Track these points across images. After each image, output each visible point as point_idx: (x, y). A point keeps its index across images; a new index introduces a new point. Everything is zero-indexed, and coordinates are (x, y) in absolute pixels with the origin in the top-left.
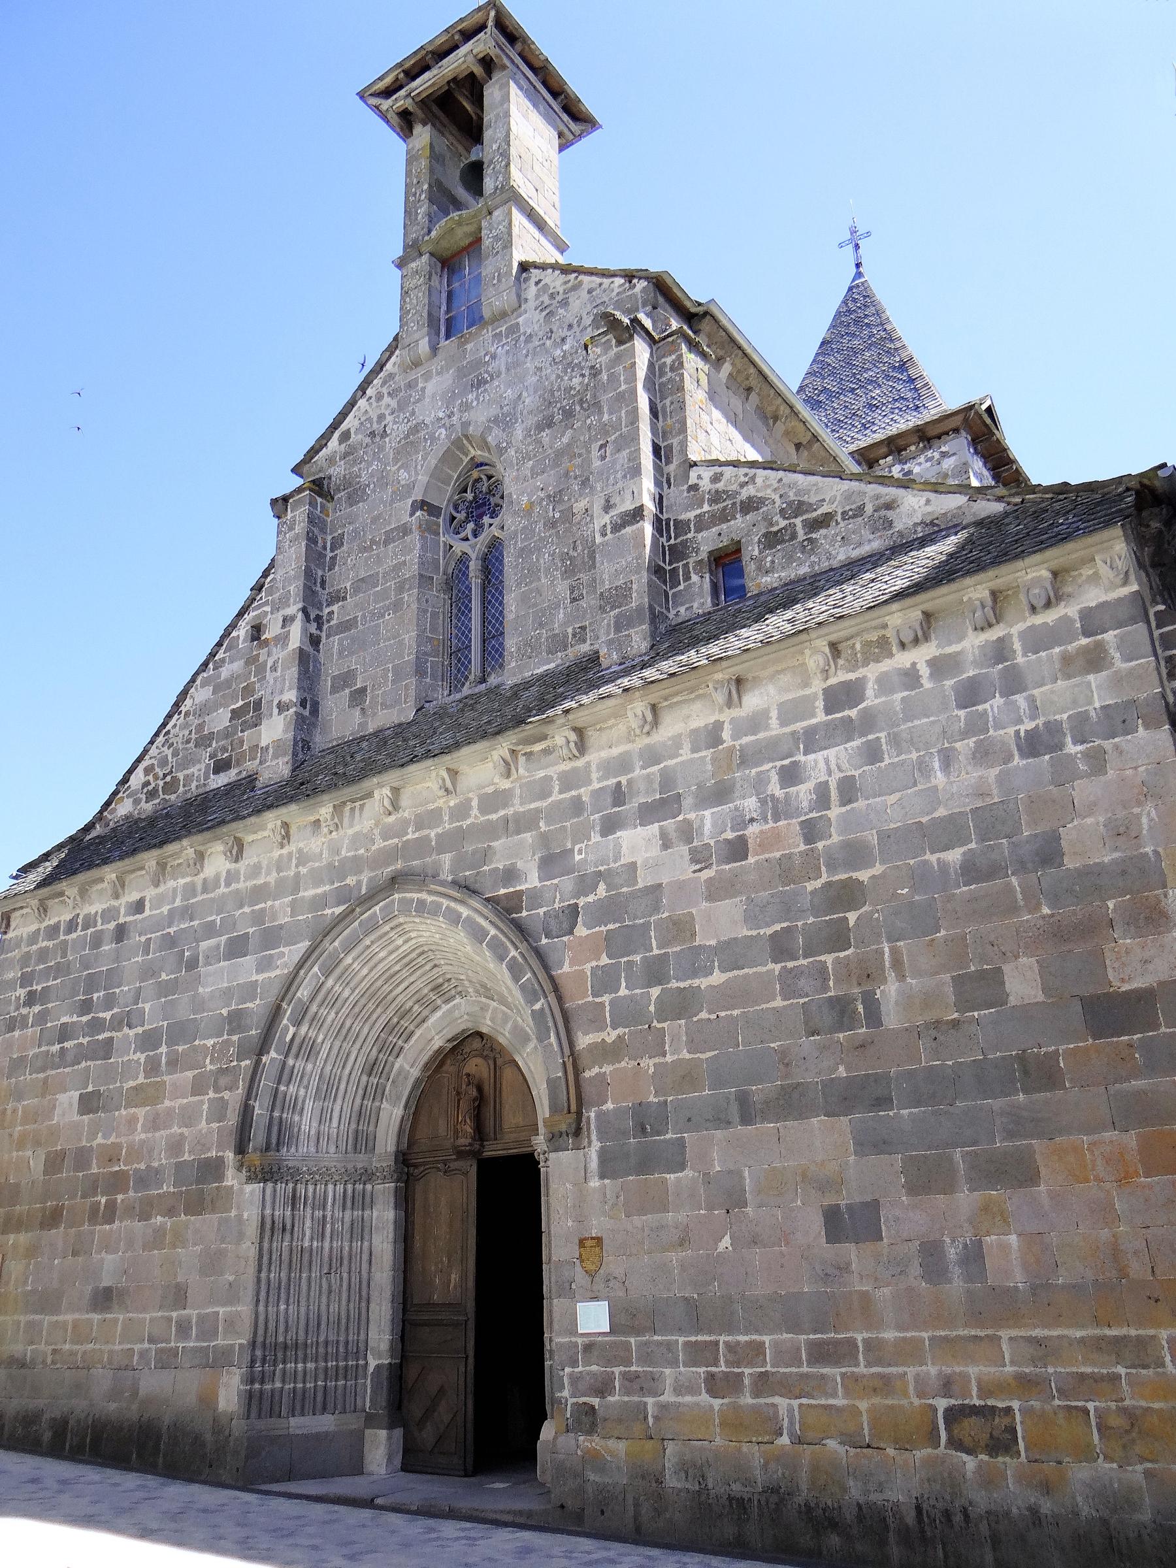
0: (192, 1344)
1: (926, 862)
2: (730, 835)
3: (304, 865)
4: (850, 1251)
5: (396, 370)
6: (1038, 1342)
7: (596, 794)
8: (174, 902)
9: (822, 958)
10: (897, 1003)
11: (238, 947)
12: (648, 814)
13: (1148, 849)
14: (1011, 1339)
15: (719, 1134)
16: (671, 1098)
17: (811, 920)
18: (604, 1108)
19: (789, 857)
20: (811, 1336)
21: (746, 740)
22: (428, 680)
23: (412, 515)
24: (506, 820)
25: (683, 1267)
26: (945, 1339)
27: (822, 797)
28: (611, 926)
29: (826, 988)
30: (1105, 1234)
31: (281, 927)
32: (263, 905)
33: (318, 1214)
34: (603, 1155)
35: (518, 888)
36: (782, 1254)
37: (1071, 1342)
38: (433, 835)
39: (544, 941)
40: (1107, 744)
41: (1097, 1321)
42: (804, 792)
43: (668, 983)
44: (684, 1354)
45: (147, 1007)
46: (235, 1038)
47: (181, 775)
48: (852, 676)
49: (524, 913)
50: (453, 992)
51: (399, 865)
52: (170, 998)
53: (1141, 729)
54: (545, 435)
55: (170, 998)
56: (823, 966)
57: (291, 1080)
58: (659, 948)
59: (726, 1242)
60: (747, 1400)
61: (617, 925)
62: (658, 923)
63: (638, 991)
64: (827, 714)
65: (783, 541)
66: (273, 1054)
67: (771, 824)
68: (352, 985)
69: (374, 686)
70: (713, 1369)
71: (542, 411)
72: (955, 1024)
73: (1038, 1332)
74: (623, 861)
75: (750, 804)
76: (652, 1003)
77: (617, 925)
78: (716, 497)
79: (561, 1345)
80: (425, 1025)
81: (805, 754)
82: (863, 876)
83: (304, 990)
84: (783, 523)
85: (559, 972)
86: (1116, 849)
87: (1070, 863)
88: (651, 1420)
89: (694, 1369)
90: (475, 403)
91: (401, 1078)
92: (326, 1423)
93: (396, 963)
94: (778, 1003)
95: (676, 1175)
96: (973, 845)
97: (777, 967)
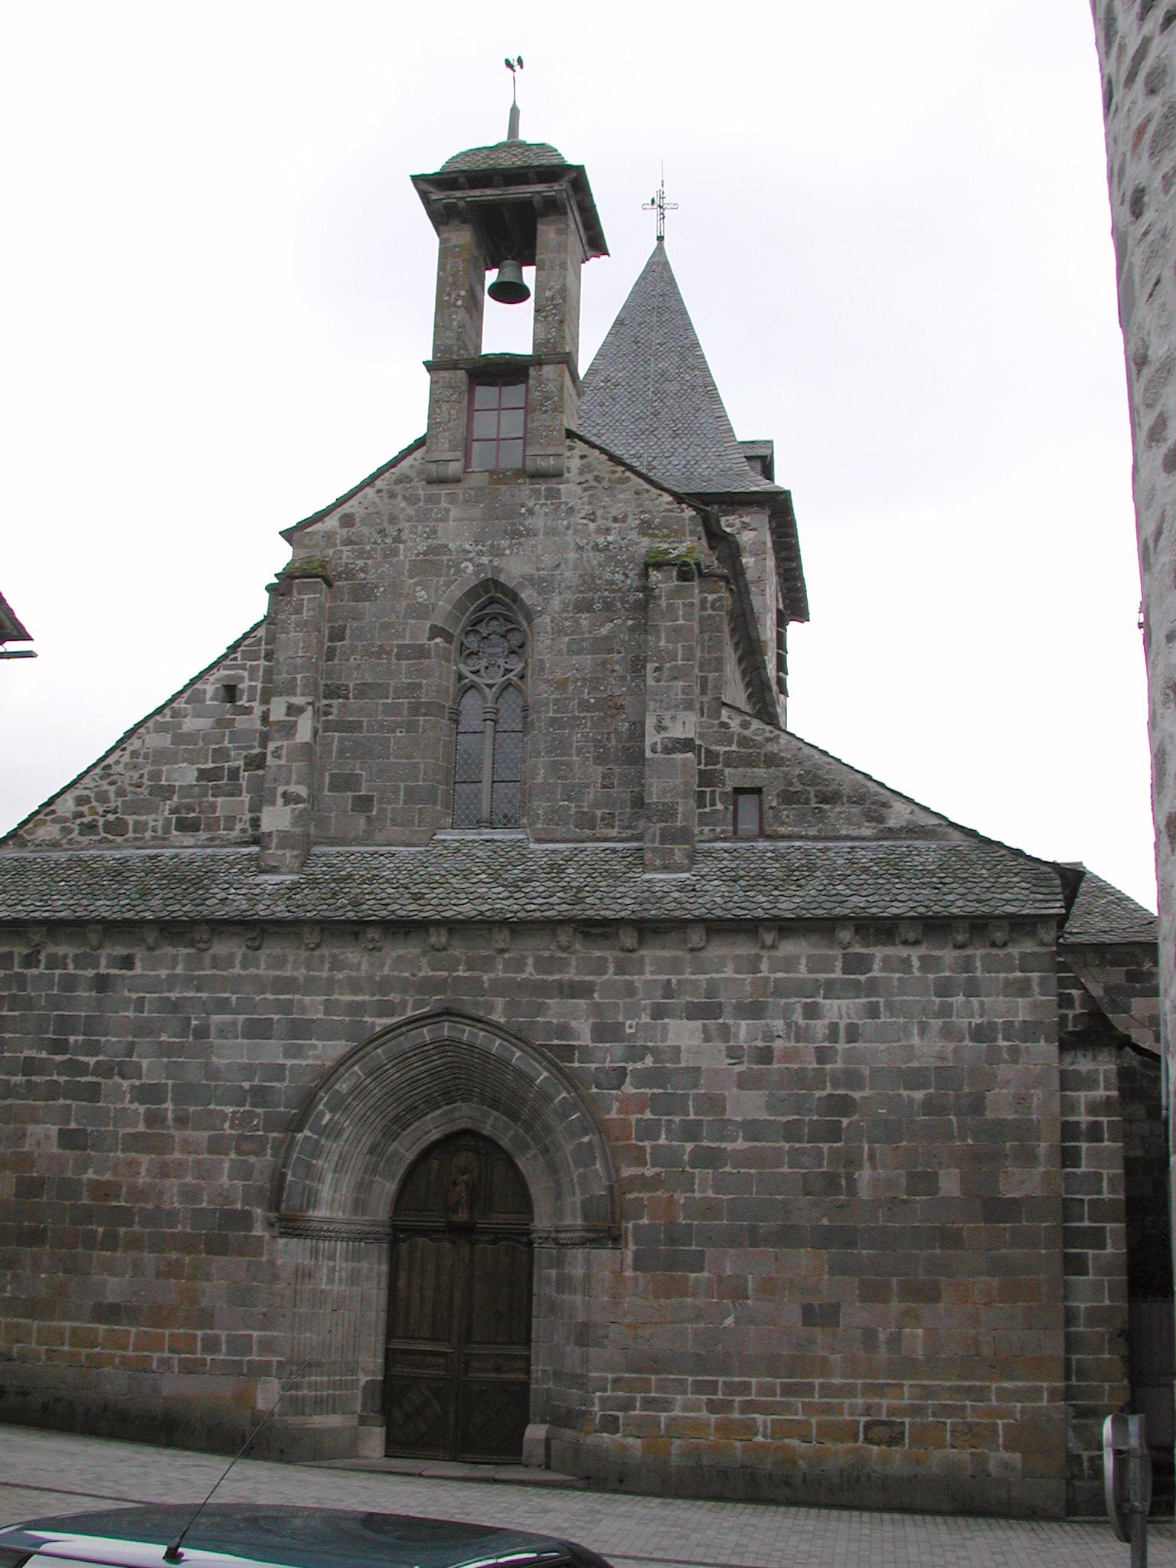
0: (222, 1357)
1: (899, 1095)
2: (760, 1044)
4: (818, 1333)
5: (412, 474)
6: (924, 1387)
8: (174, 968)
9: (821, 1145)
10: (869, 1183)
11: (258, 1030)
12: (695, 1012)
13: (1034, 1117)
14: (911, 1386)
15: (732, 1251)
17: (815, 1118)
19: (804, 1070)
20: (785, 1380)
21: (779, 975)
22: (438, 808)
23: (431, 638)
24: (560, 984)
26: (871, 1384)
27: (833, 1032)
28: (655, 1091)
29: (820, 1165)
30: (972, 1332)
31: (313, 1021)
33: (331, 1263)
34: (637, 1255)
36: (770, 1331)
37: (944, 1388)
38: (485, 978)
39: (594, 1090)
40: (1023, 1046)
41: (960, 1377)
42: (820, 1027)
45: (145, 1063)
46: (259, 1110)
47: (130, 819)
48: (865, 951)
52: (174, 1059)
53: (1042, 1041)
54: (585, 620)
55: (174, 1059)
56: (820, 1150)
59: (729, 1321)
60: (736, 1415)
61: (661, 1091)
62: (696, 1097)
63: (674, 1143)
64: (844, 973)
65: (798, 802)
66: (307, 1132)
67: (793, 1043)
69: (382, 798)
70: (713, 1397)
71: (581, 592)
72: (904, 1202)
73: (925, 1382)
74: (669, 1043)
75: (778, 1025)
77: (661, 1091)
78: (744, 742)
81: (824, 998)
82: (856, 1095)
83: (344, 1082)
84: (799, 787)
86: (1016, 1112)
87: (989, 1115)
90: (508, 552)
92: (335, 1420)
94: (786, 1169)
96: (932, 1091)
97: (787, 1146)
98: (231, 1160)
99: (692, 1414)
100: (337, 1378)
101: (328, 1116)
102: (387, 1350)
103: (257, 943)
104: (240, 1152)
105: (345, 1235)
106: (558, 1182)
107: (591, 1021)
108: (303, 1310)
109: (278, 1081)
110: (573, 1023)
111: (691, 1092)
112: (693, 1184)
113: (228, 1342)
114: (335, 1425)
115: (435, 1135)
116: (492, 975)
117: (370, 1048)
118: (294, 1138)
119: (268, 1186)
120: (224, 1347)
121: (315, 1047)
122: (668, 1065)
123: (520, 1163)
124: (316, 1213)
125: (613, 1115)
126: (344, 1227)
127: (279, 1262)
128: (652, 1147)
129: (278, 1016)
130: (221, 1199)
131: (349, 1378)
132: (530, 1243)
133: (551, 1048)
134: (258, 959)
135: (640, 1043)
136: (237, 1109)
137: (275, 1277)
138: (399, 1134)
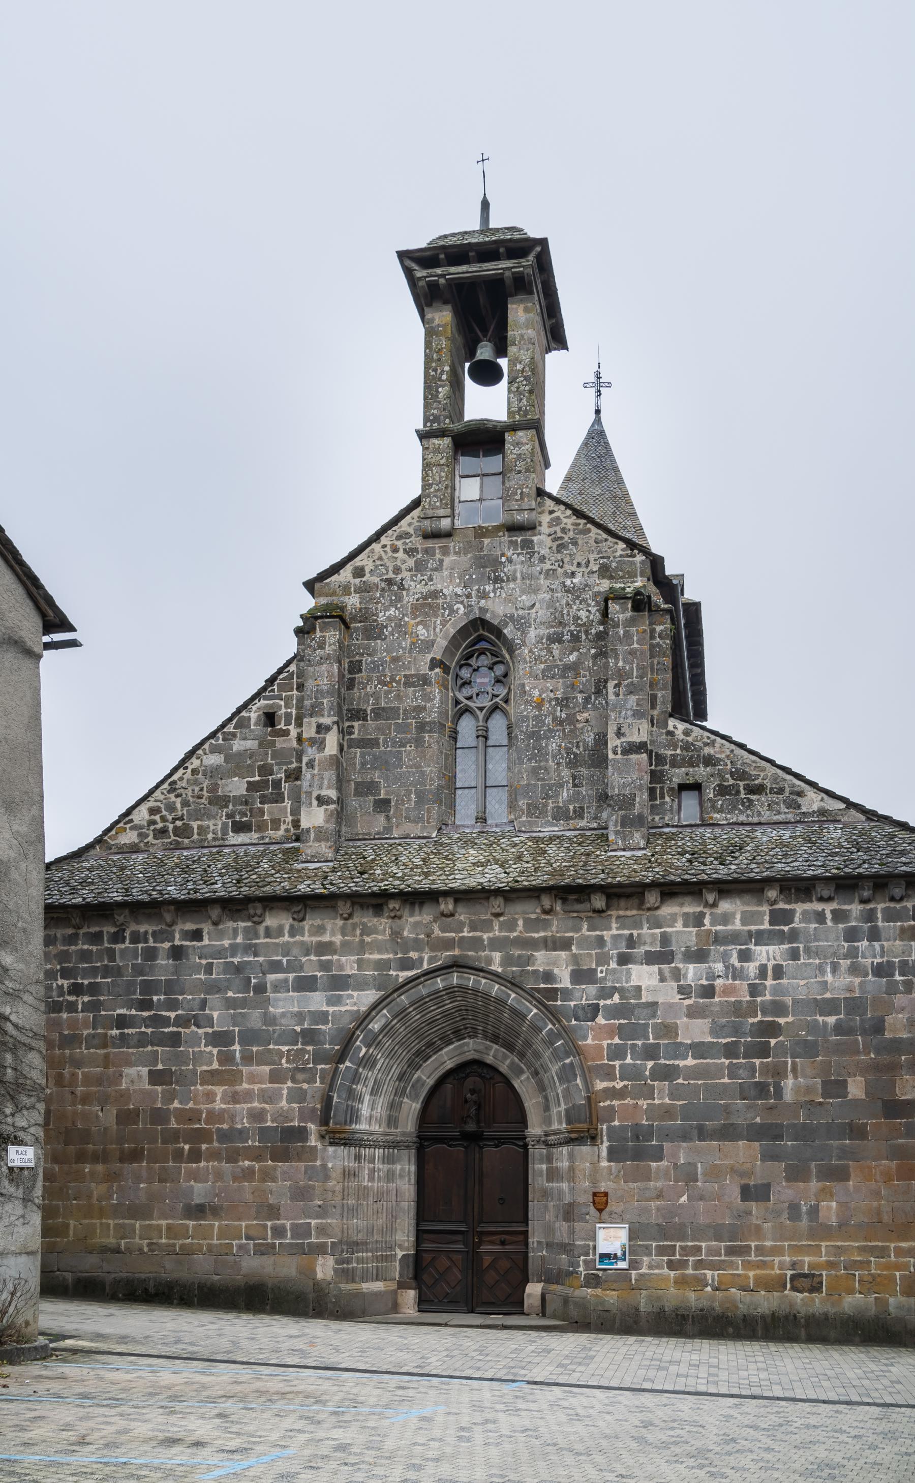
3: (368, 935)
7: (615, 938)
24: (545, 939)
25: (658, 1209)
32: (329, 957)
33: (371, 1166)
35: (554, 986)
46: (310, 1048)
49: (559, 1003)
51: (457, 952)
58: (654, 1039)
61: (626, 1021)
63: (639, 1062)
66: (348, 1064)
74: (632, 984)
77: (626, 1021)
79: (580, 1245)
88: (633, 1281)
91: (419, 1085)
98: (288, 1087)
99: (656, 1271)
101: (364, 1050)
102: (418, 1231)
103: (301, 915)
104: (294, 1081)
106: (546, 1098)
107: (570, 968)
108: (351, 1202)
112: (654, 1093)
113: (291, 1230)
115: (449, 1065)
116: (491, 935)
117: (395, 995)
118: (337, 1068)
119: (319, 1106)
120: (289, 1233)
121: (352, 997)
124: (357, 1127)
125: (589, 1041)
126: (380, 1138)
127: (330, 1165)
128: (620, 1066)
130: (282, 1118)
132: (525, 1146)
133: (538, 990)
134: (303, 928)
135: (609, 984)
136: (291, 1048)
137: (327, 1178)
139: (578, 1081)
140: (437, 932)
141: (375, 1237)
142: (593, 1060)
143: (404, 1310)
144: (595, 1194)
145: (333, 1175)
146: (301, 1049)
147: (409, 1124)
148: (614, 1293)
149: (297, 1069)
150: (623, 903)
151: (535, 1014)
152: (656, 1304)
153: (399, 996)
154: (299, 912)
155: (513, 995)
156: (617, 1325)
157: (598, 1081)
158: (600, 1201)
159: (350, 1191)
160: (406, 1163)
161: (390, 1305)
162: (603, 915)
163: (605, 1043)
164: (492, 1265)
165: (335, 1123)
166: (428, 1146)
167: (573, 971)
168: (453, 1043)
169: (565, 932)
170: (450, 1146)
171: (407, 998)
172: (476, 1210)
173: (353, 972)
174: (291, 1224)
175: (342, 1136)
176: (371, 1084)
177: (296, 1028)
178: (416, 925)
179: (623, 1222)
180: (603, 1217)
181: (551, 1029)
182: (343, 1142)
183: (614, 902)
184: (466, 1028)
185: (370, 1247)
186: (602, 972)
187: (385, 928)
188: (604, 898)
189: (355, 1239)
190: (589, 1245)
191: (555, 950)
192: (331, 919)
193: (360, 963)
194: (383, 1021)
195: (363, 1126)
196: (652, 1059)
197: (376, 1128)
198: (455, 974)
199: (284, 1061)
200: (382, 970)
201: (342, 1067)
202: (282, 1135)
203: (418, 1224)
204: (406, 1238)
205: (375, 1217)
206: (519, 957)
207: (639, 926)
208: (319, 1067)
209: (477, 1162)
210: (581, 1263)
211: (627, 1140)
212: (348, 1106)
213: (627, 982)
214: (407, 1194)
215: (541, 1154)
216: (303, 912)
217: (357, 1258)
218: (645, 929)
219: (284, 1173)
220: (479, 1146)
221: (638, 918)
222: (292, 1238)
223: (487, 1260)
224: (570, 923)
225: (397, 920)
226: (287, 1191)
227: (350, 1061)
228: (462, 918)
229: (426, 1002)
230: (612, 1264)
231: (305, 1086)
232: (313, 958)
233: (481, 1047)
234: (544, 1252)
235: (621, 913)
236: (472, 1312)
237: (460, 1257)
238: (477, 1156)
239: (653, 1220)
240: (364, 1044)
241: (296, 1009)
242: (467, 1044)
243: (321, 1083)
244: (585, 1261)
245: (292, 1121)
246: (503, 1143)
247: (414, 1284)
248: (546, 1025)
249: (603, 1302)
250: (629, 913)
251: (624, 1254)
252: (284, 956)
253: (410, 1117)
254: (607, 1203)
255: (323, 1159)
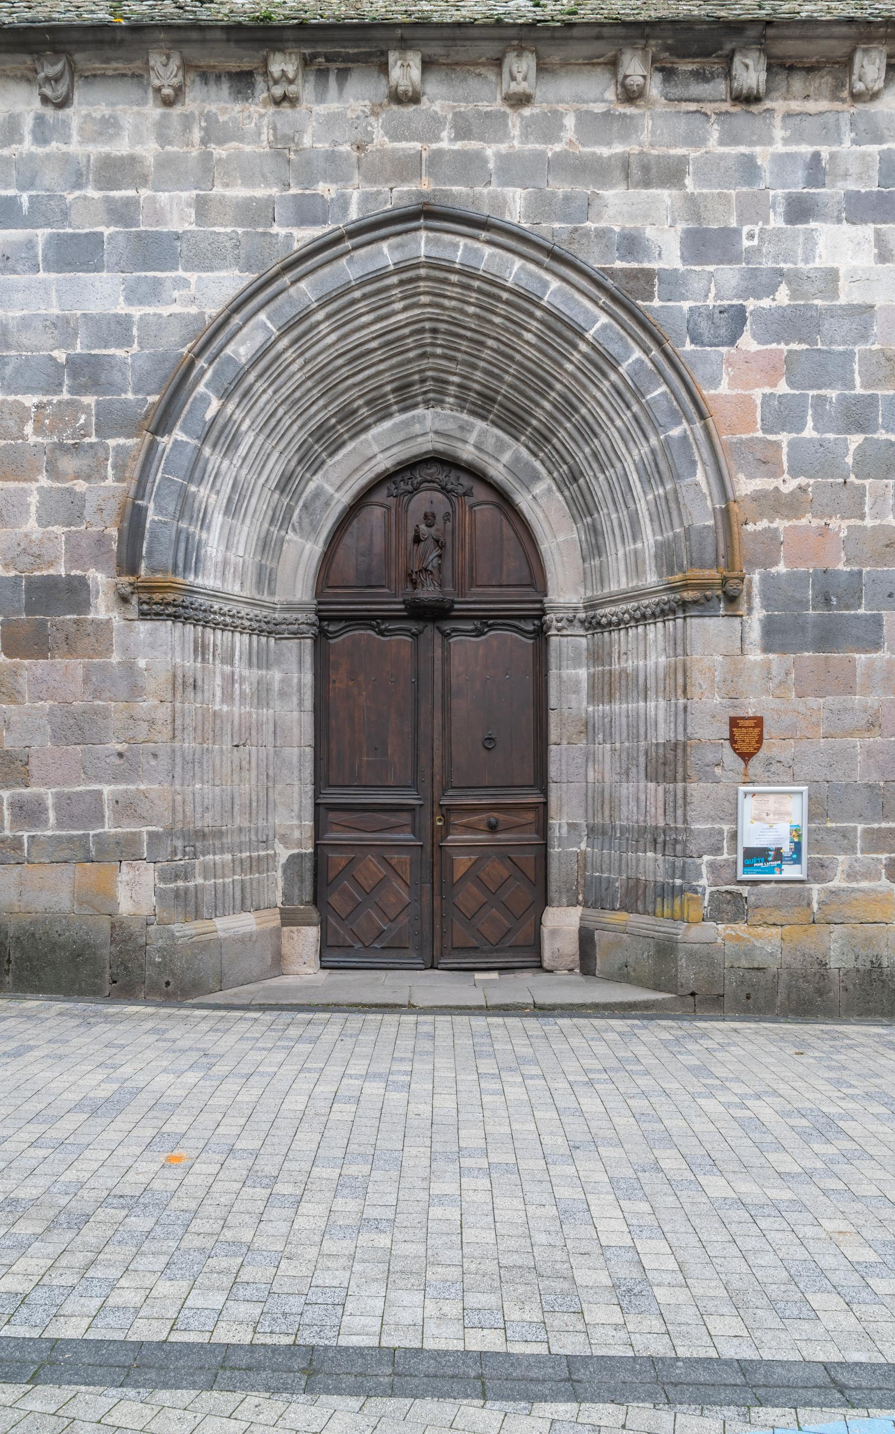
0: (49, 833)
3: (220, 142)
7: (780, 160)
16: (868, 569)
18: (773, 570)
24: (625, 163)
25: (869, 754)
32: (131, 193)
33: (227, 668)
35: (646, 265)
39: (689, 347)
43: (875, 432)
44: (862, 841)
46: (89, 400)
49: (656, 303)
50: (420, 399)
51: (426, 185)
57: (203, 478)
58: (864, 386)
61: (805, 346)
63: (831, 436)
66: (178, 434)
68: (308, 355)
74: (817, 263)
76: (851, 452)
77: (805, 346)
79: (701, 832)
80: (363, 437)
83: (243, 343)
85: (712, 392)
88: (815, 906)
89: (874, 856)
91: (319, 504)
93: (374, 339)
95: (868, 655)
98: (41, 490)
99: (865, 884)
100: (245, 855)
101: (215, 404)
102: (317, 805)
103: (62, 89)
104: (54, 472)
105: (247, 623)
106: (595, 530)
107: (681, 226)
108: (189, 745)
109: (119, 346)
110: (650, 232)
111: (857, 349)
112: (862, 504)
113: (58, 808)
114: (248, 929)
115: (384, 463)
116: (503, 148)
117: (287, 279)
118: (153, 446)
119: (114, 532)
120: (52, 815)
121: (185, 283)
122: (817, 302)
123: (523, 501)
124: (199, 581)
125: (724, 388)
126: (245, 610)
127: (142, 663)
128: (791, 444)
129: (112, 229)
130: (27, 559)
131: (262, 853)
132: (541, 635)
133: (611, 273)
134: (65, 124)
135: (768, 264)
136: (45, 399)
137: (135, 691)
138: (323, 462)
139: (700, 476)
140: (380, 139)
141: (237, 822)
142: (732, 430)
143: (296, 968)
144: (734, 722)
145: (151, 685)
146: (69, 403)
147: (299, 585)
148: (774, 930)
149: (60, 447)
150: (798, 83)
151: (605, 327)
152: (863, 953)
153: (294, 283)
154: (57, 79)
155: (555, 284)
156: (780, 999)
157: (741, 477)
158: (746, 738)
159: (188, 721)
160: (295, 667)
161: (269, 960)
162: (755, 108)
163: (758, 394)
164: (472, 874)
165: (154, 570)
166: (337, 634)
167: (688, 232)
168: (390, 415)
169: (669, 146)
170: (381, 633)
171: (314, 287)
172: (437, 762)
173: (187, 227)
174: (58, 796)
175: (170, 597)
176: (227, 490)
177: (55, 353)
178: (331, 121)
179: (794, 780)
180: (751, 771)
181: (639, 361)
182: (171, 610)
183: (780, 79)
184: (423, 381)
185: (227, 840)
186: (751, 236)
187: (258, 127)
188: (763, 63)
189: (199, 825)
190: (721, 832)
191: (647, 184)
192: (131, 103)
193: (202, 206)
194: (259, 339)
195: (208, 580)
196: (861, 428)
197: (234, 588)
198: (423, 234)
199: (29, 429)
200: (254, 223)
201: (165, 442)
202: (28, 598)
203: (317, 794)
204: (296, 822)
205: (236, 777)
206: (567, 198)
207: (831, 135)
208: (112, 442)
209: (438, 664)
210: (704, 869)
211: (802, 604)
212: (179, 532)
213: (806, 261)
214: (296, 731)
215: (576, 648)
216: (66, 80)
217: (205, 866)
218: (847, 143)
219: (36, 681)
220: (442, 632)
221: (831, 119)
222: (60, 825)
223: (462, 863)
224: (682, 126)
225: (286, 108)
226: (44, 721)
227: (184, 430)
228: (437, 107)
229: (353, 302)
230: (771, 871)
231: (81, 486)
232: (92, 193)
233: (450, 427)
234: (583, 846)
235: (795, 105)
236: (432, 967)
237: (406, 857)
238: (438, 652)
239: (859, 777)
240: (216, 391)
241: (55, 311)
242: (421, 419)
243: (119, 479)
244: (712, 865)
245: (51, 564)
246: (491, 627)
247: (315, 916)
248: (628, 351)
249: (749, 953)
250: (811, 106)
251: (797, 848)
252: (23, 188)
253: (301, 572)
254: (760, 741)
255: (126, 650)
